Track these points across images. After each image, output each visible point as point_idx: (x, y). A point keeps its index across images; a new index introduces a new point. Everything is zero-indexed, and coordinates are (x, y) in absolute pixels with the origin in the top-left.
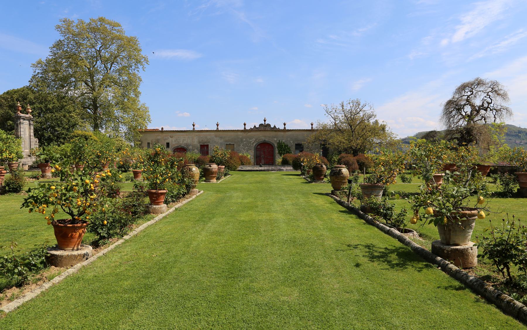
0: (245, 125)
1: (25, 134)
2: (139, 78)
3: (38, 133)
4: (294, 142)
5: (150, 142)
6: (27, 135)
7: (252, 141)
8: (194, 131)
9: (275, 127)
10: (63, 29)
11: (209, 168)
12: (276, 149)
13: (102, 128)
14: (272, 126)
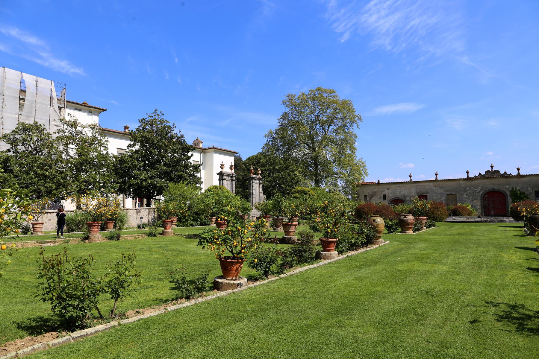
0: (468, 172)
1: (256, 192)
2: (354, 135)
3: (268, 191)
4: (532, 189)
5: (367, 195)
6: (258, 192)
7: (478, 189)
8: (411, 182)
9: (505, 173)
10: (288, 103)
11: (405, 219)
12: (509, 198)
13: (322, 183)
14: (502, 172)
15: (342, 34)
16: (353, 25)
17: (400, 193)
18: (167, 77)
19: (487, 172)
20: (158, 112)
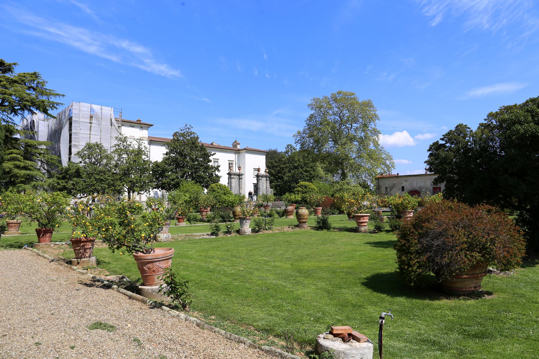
1: (263, 187)
6: (265, 187)
15: (434, 17)
16: (447, 6)
18: (256, 73)
20: (188, 126)
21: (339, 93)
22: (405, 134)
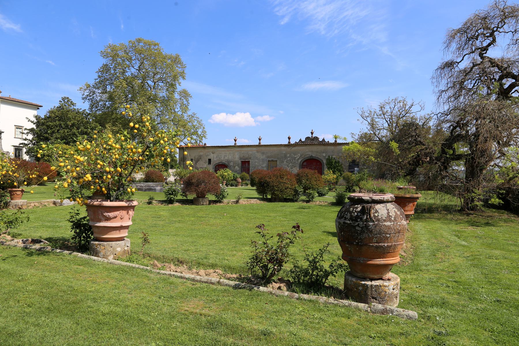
0: (289, 138)
7: (298, 156)
8: (235, 146)
9: (323, 140)
12: (325, 166)
14: (321, 140)
15: (283, 17)
16: (295, 9)
17: (224, 157)
19: (307, 138)
21: (139, 41)
22: (248, 115)
